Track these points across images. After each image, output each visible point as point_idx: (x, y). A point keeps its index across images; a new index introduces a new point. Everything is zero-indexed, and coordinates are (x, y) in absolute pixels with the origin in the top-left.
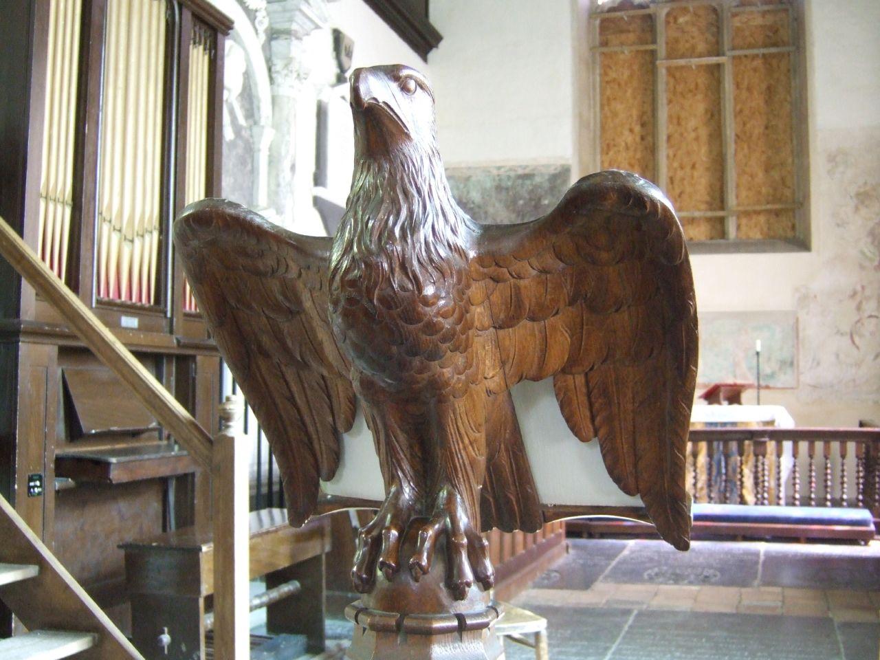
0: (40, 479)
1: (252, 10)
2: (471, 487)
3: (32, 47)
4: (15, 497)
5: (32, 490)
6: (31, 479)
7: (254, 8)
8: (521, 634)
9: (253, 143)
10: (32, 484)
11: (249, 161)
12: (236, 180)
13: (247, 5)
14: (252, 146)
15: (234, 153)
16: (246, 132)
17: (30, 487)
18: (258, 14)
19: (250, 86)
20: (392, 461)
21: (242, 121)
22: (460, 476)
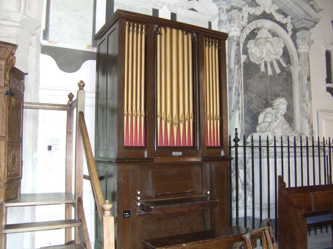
0: (129, 212)
1: (285, 24)
2: (107, 115)
3: (222, 81)
4: (324, 214)
5: (125, 216)
6: (125, 212)
7: (286, 23)
8: (308, 92)
9: (291, 72)
10: (124, 214)
11: (290, 79)
12: (283, 87)
13: (281, 23)
14: (291, 73)
15: (282, 77)
16: (287, 69)
17: (124, 215)
18: (287, 25)
19: (288, 51)
20: (10, 167)
21: (284, 65)
22: (208, 172)
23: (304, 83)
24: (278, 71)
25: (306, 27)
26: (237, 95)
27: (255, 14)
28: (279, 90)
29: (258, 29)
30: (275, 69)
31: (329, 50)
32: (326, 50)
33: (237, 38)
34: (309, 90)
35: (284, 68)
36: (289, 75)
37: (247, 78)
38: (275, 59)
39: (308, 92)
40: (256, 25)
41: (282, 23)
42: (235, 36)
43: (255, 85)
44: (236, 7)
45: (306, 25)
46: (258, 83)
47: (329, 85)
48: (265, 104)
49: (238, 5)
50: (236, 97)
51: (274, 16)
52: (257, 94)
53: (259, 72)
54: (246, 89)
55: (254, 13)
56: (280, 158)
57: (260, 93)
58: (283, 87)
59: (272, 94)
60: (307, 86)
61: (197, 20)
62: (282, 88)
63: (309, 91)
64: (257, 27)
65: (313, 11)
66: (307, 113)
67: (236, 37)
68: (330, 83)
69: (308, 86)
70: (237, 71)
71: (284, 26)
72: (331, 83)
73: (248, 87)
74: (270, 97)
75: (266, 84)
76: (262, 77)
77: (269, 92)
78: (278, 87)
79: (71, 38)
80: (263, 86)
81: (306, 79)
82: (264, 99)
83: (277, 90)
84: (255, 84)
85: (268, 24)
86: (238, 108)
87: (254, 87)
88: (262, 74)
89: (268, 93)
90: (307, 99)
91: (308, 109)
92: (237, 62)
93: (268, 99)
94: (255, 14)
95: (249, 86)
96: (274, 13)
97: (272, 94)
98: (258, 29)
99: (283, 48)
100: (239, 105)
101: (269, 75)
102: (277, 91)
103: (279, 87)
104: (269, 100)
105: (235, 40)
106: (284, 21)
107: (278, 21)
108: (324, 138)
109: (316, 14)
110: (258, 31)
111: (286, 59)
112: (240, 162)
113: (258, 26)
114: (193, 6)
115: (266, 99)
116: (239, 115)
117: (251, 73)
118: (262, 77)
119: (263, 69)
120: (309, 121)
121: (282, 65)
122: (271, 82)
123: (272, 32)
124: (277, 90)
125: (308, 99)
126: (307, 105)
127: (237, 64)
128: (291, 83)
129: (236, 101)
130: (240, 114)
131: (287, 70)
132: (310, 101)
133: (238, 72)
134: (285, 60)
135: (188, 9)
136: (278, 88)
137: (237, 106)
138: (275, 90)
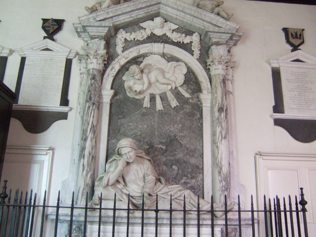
12: (184, 125)
23: (214, 115)
24: (174, 103)
25: (218, 42)
26: (83, 140)
27: (136, 40)
28: (175, 130)
29: (144, 56)
30: (169, 103)
31: (277, 68)
32: (271, 68)
33: (93, 71)
34: (221, 125)
35: (188, 99)
36: (198, 108)
37: (119, 118)
38: (170, 90)
39: (219, 128)
40: (138, 51)
41: (183, 42)
42: (90, 69)
43: (131, 126)
44: (96, 36)
45: (218, 39)
46: (136, 123)
47: (279, 116)
48: (148, 149)
49: (98, 34)
50: (83, 142)
51: (169, 37)
52: (134, 137)
53: (141, 108)
54: (117, 131)
55: (134, 39)
56: (242, 218)
57: (140, 135)
58: (184, 125)
59: (161, 135)
60: (218, 119)
61: (51, 60)
62: (182, 127)
63: (220, 127)
64: (139, 53)
65: (221, 20)
66: (218, 159)
67: (91, 70)
68: (283, 113)
69: (220, 120)
70: (87, 111)
71: (187, 47)
72: (282, 112)
73: (120, 129)
74: (157, 139)
75: (151, 123)
76: (144, 115)
77: (156, 133)
78: (173, 125)
79: (47, 97)
80: (145, 126)
81: (217, 110)
82: (147, 142)
83: (172, 129)
84: (131, 124)
85: (158, 47)
86: (83, 156)
87: (129, 128)
88: (145, 111)
89: (155, 134)
90: (217, 138)
91: (218, 153)
92: (88, 100)
93: (153, 143)
94: (136, 40)
95: (122, 128)
96: (169, 34)
97: (161, 135)
98: (144, 56)
99: (185, 75)
100: (84, 152)
101: (157, 110)
102: (172, 132)
103: (176, 126)
104: (155, 143)
105: (90, 74)
106: (187, 40)
107: (176, 41)
108: (265, 197)
109: (228, 23)
110: (143, 59)
111: (192, 87)
112: (77, 227)
113: (141, 53)
114: (47, 46)
115: (151, 142)
116: (83, 165)
117: (126, 110)
118: (144, 115)
119: (147, 103)
120: (220, 171)
121: (184, 96)
122: (162, 119)
123: (169, 56)
124: (171, 129)
125: (219, 139)
126: (217, 147)
127: (88, 102)
128: (199, 118)
129: (82, 147)
130: (85, 164)
131: (193, 101)
132: (221, 140)
133: (88, 111)
134: (191, 89)
135: (41, 50)
136: (174, 127)
137: (82, 153)
138: (168, 129)
